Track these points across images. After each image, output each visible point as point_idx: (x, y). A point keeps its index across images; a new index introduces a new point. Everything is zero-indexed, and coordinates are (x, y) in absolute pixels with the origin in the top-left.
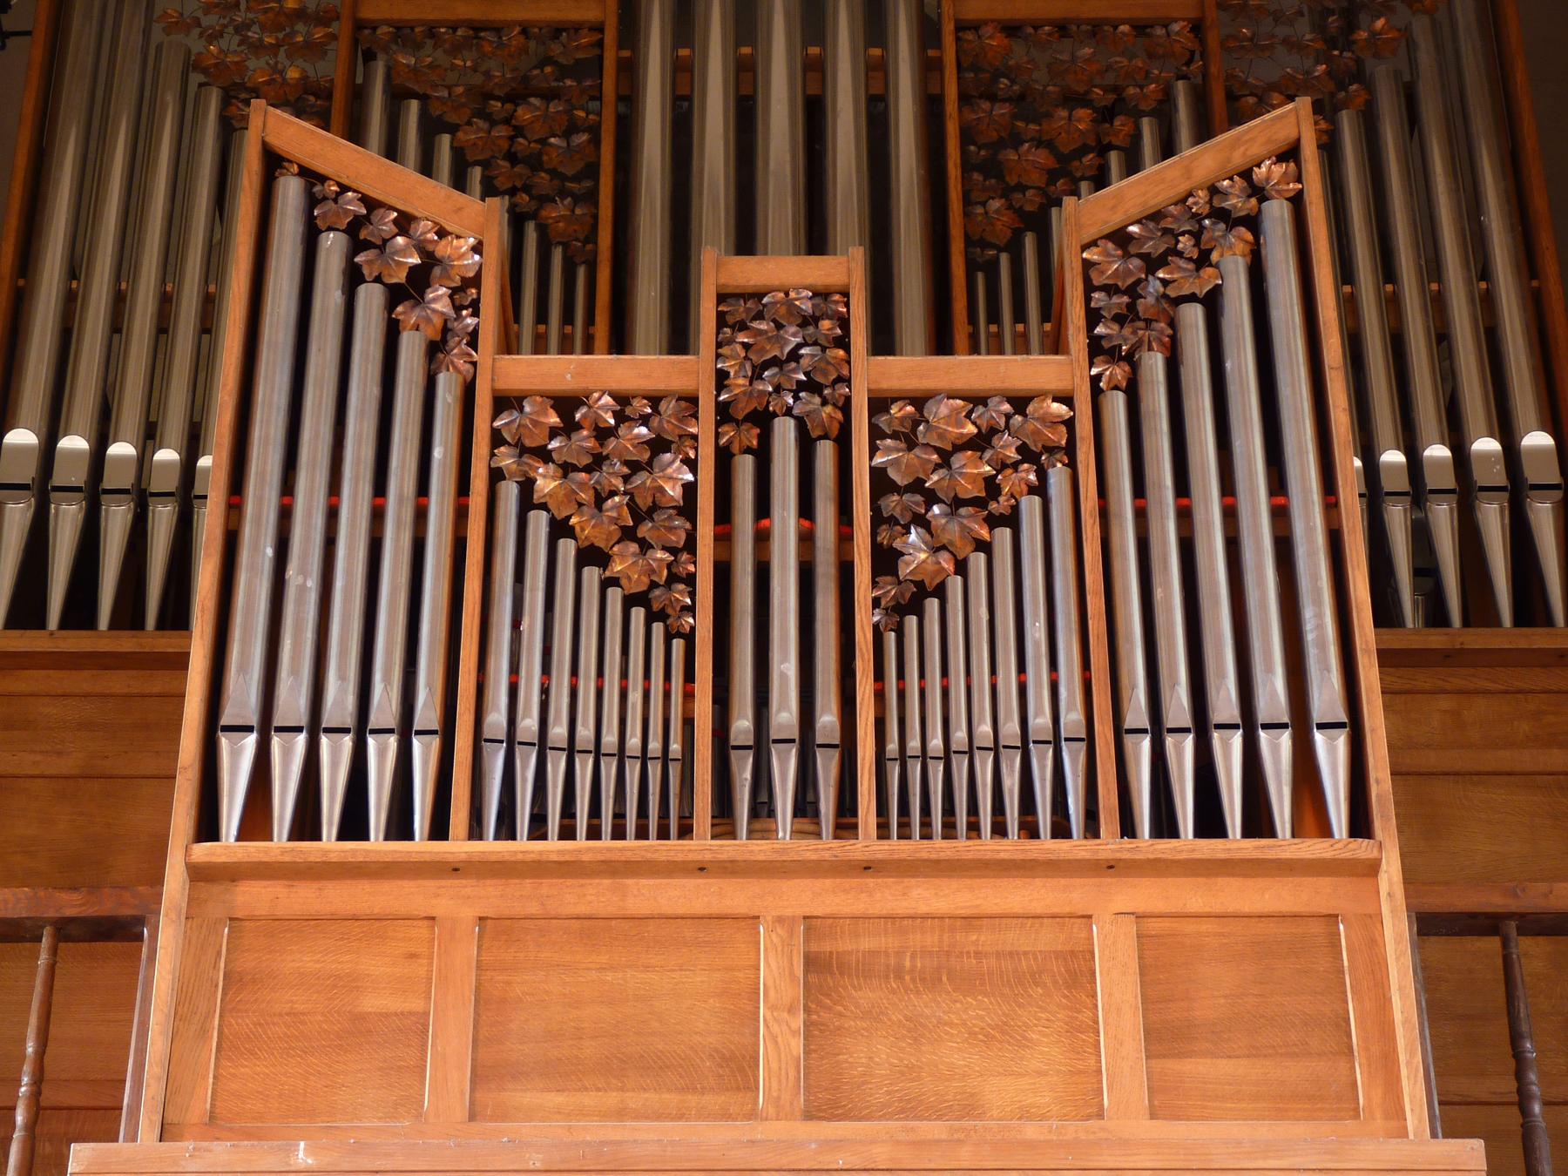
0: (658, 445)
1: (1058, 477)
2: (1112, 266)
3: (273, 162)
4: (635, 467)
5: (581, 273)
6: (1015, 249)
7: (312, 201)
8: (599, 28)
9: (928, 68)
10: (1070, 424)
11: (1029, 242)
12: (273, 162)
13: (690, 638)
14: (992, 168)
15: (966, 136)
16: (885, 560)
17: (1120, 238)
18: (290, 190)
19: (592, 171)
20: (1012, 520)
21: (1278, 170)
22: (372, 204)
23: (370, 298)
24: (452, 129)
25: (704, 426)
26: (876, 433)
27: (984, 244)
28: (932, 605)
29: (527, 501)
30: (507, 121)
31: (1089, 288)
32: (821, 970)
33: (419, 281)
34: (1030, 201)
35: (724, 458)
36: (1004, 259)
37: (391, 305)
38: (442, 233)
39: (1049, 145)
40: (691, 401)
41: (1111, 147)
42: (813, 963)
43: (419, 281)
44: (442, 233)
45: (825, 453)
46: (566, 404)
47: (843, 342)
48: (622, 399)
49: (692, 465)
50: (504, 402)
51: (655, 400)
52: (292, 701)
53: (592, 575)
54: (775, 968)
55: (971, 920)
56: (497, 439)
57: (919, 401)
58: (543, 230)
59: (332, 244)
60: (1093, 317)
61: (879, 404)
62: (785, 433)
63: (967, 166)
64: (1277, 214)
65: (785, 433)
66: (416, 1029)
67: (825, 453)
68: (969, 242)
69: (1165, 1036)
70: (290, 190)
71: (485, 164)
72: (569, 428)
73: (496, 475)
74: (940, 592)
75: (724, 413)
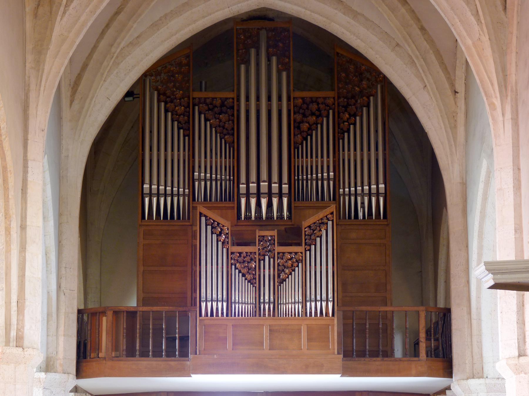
0: (251, 259)
1: (300, 265)
2: (308, 231)
3: (201, 214)
4: (248, 262)
5: (232, 149)
6: (302, 144)
7: (206, 220)
8: (233, 99)
9: (288, 105)
10: (302, 256)
11: (304, 142)
12: (201, 214)
13: (256, 287)
14: (299, 128)
15: (295, 121)
16: (279, 276)
17: (309, 227)
18: (203, 219)
19: (233, 129)
20: (294, 270)
21: (330, 216)
22: (214, 221)
23: (215, 236)
24: (210, 120)
25: (257, 256)
26: (278, 258)
27: (297, 143)
28: (284, 282)
29: (236, 268)
30: (218, 119)
31: (305, 235)
32: (271, 331)
33: (221, 233)
34: (305, 134)
35: (259, 261)
36: (300, 146)
37: (217, 236)
38: (223, 226)
39: (308, 123)
40: (255, 253)
41: (318, 124)
42: (270, 330)
43: (221, 233)
44: (223, 226)
45: (272, 260)
46: (240, 253)
47: (274, 244)
48: (247, 253)
49: (255, 262)
50: (232, 253)
51: (251, 253)
52: (209, 297)
53: (244, 278)
54: (265, 331)
55: (288, 325)
56: (231, 259)
57: (284, 253)
58: (225, 141)
59: (209, 227)
60: (305, 240)
61: (278, 253)
62: (267, 258)
63: (294, 127)
64: (330, 223)
65: (267, 258)
66: (225, 339)
67: (272, 260)
68: (294, 143)
69: (309, 340)
70: (203, 219)
71: (215, 128)
72: (240, 256)
73: (232, 264)
74: (285, 281)
75: (259, 254)
